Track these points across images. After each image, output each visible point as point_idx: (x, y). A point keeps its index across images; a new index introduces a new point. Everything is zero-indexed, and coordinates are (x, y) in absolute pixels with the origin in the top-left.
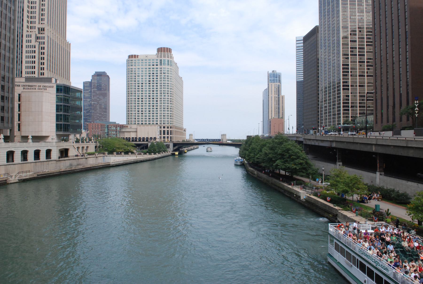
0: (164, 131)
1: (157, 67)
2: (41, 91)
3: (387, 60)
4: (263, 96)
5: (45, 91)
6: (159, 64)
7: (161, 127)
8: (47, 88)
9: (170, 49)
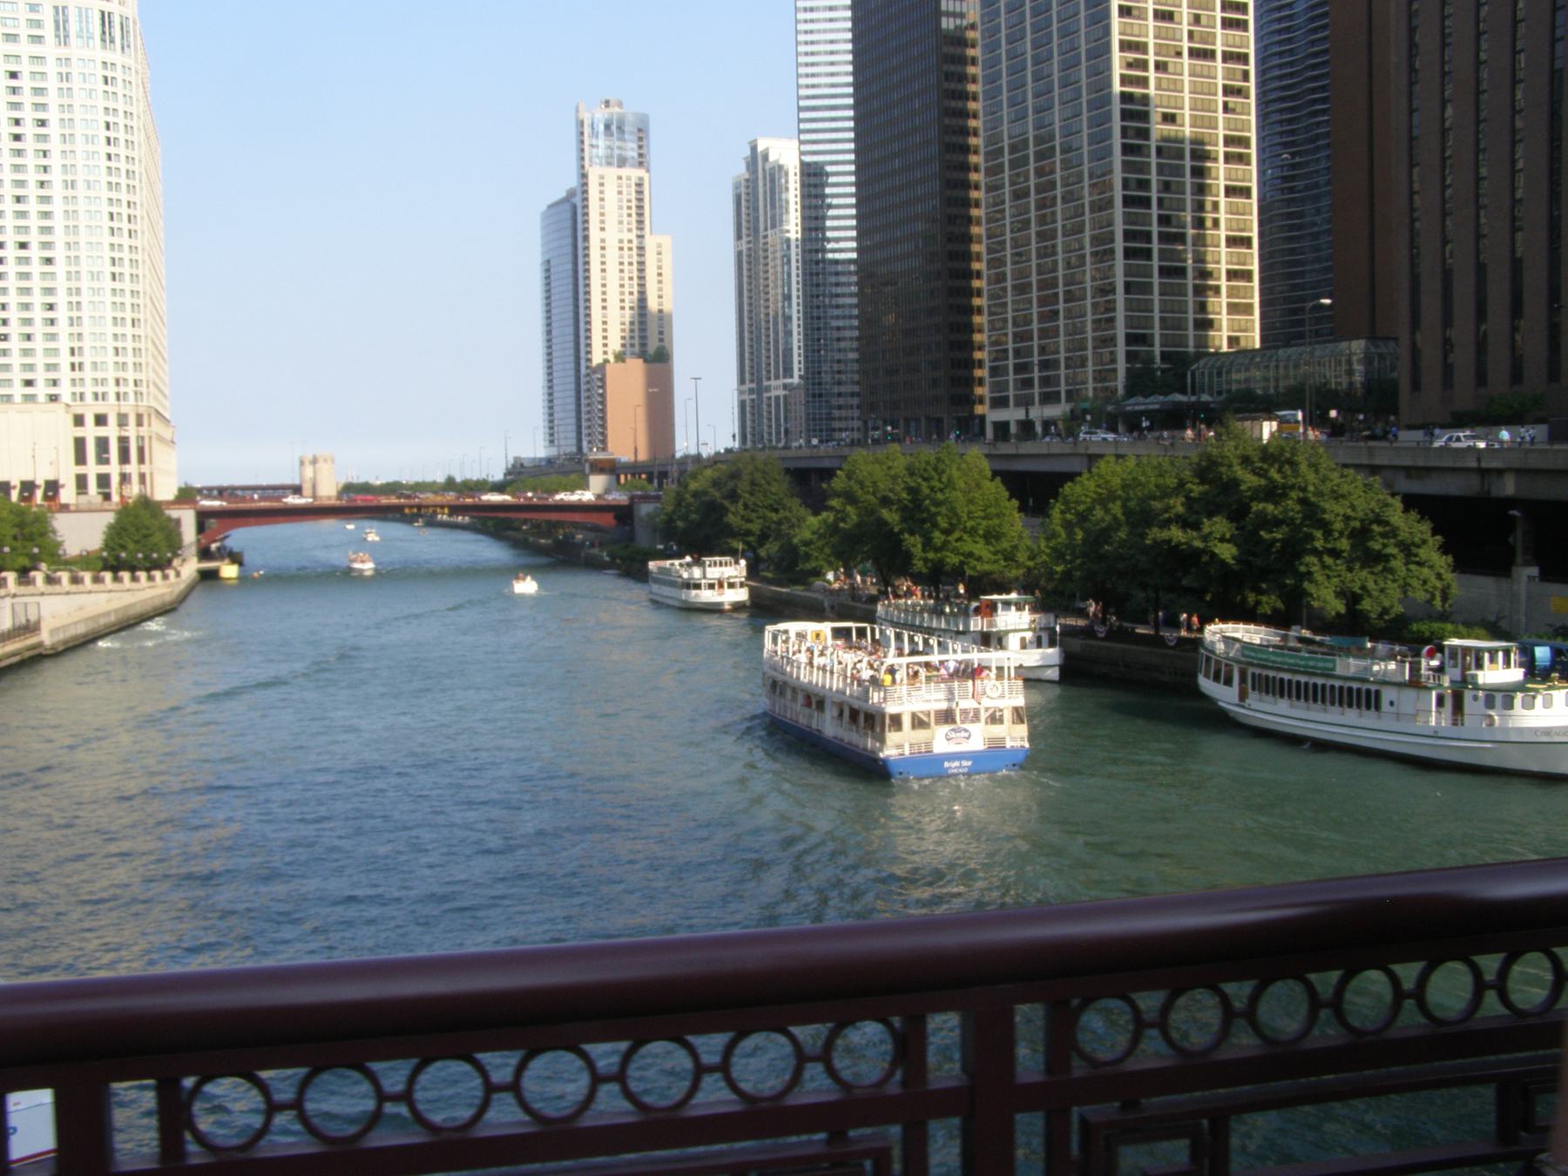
0: (102, 444)
1: (37, 50)
3: (1478, 93)
4: (546, 244)
6: (48, 31)
7: (79, 420)
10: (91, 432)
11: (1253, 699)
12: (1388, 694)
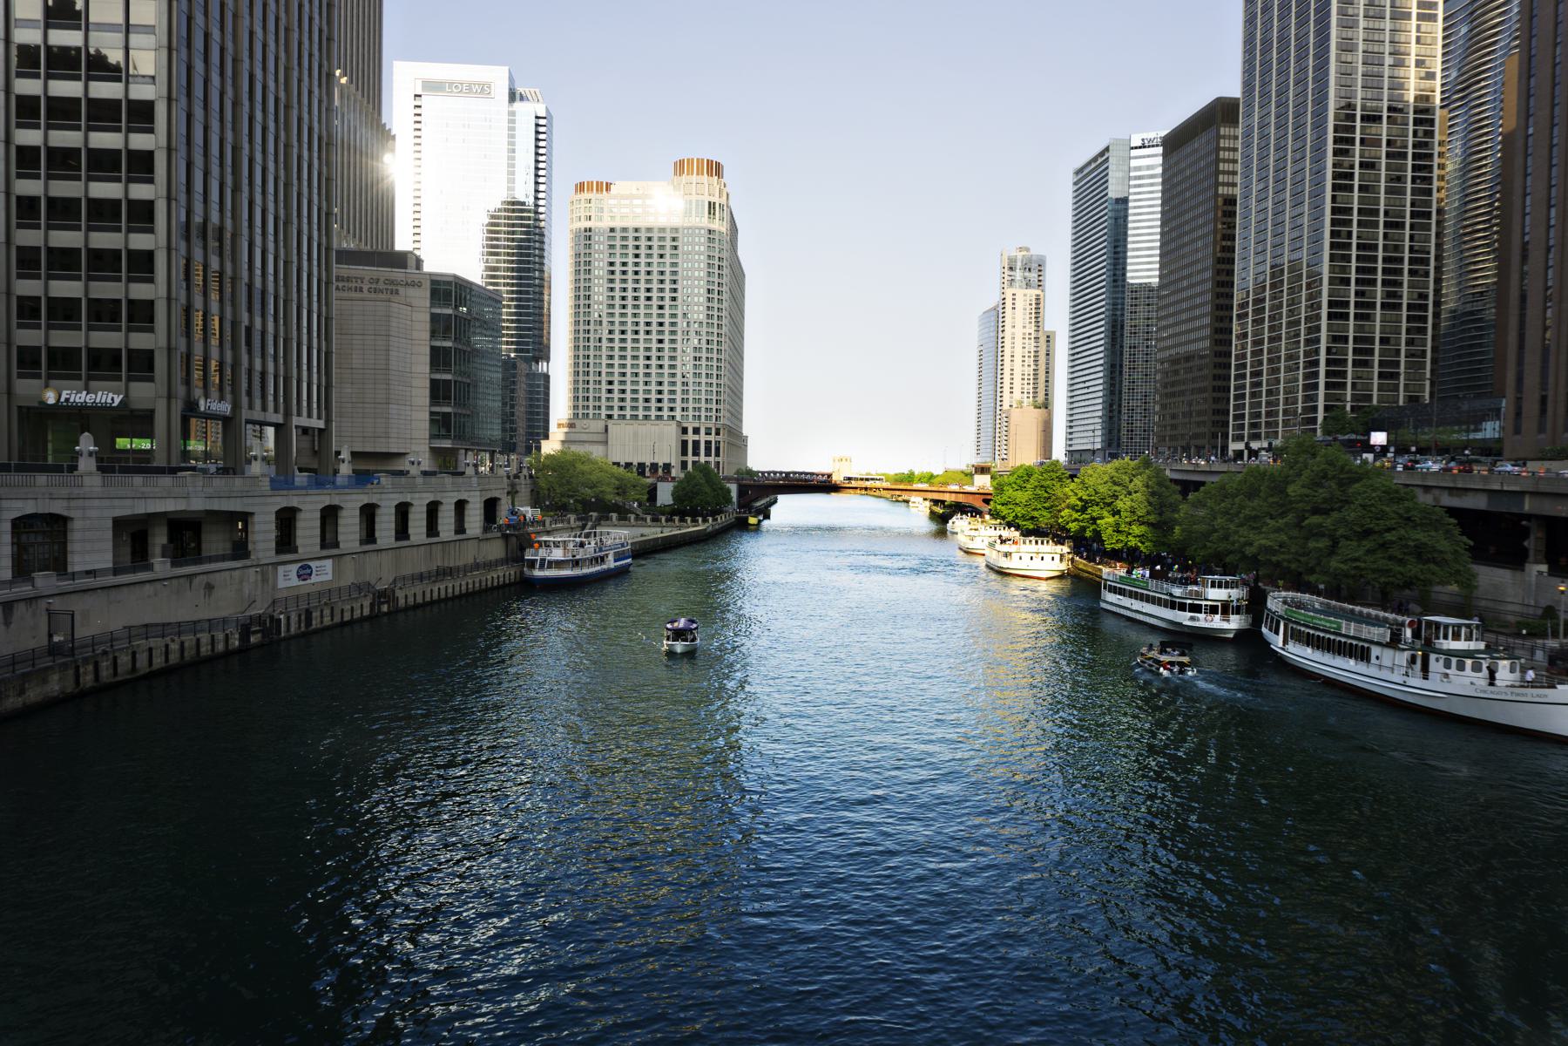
0: (696, 444)
2: (381, 296)
5: (394, 298)
8: (402, 290)
9: (718, 164)
10: (691, 437)
11: (1291, 647)
12: (1375, 651)
